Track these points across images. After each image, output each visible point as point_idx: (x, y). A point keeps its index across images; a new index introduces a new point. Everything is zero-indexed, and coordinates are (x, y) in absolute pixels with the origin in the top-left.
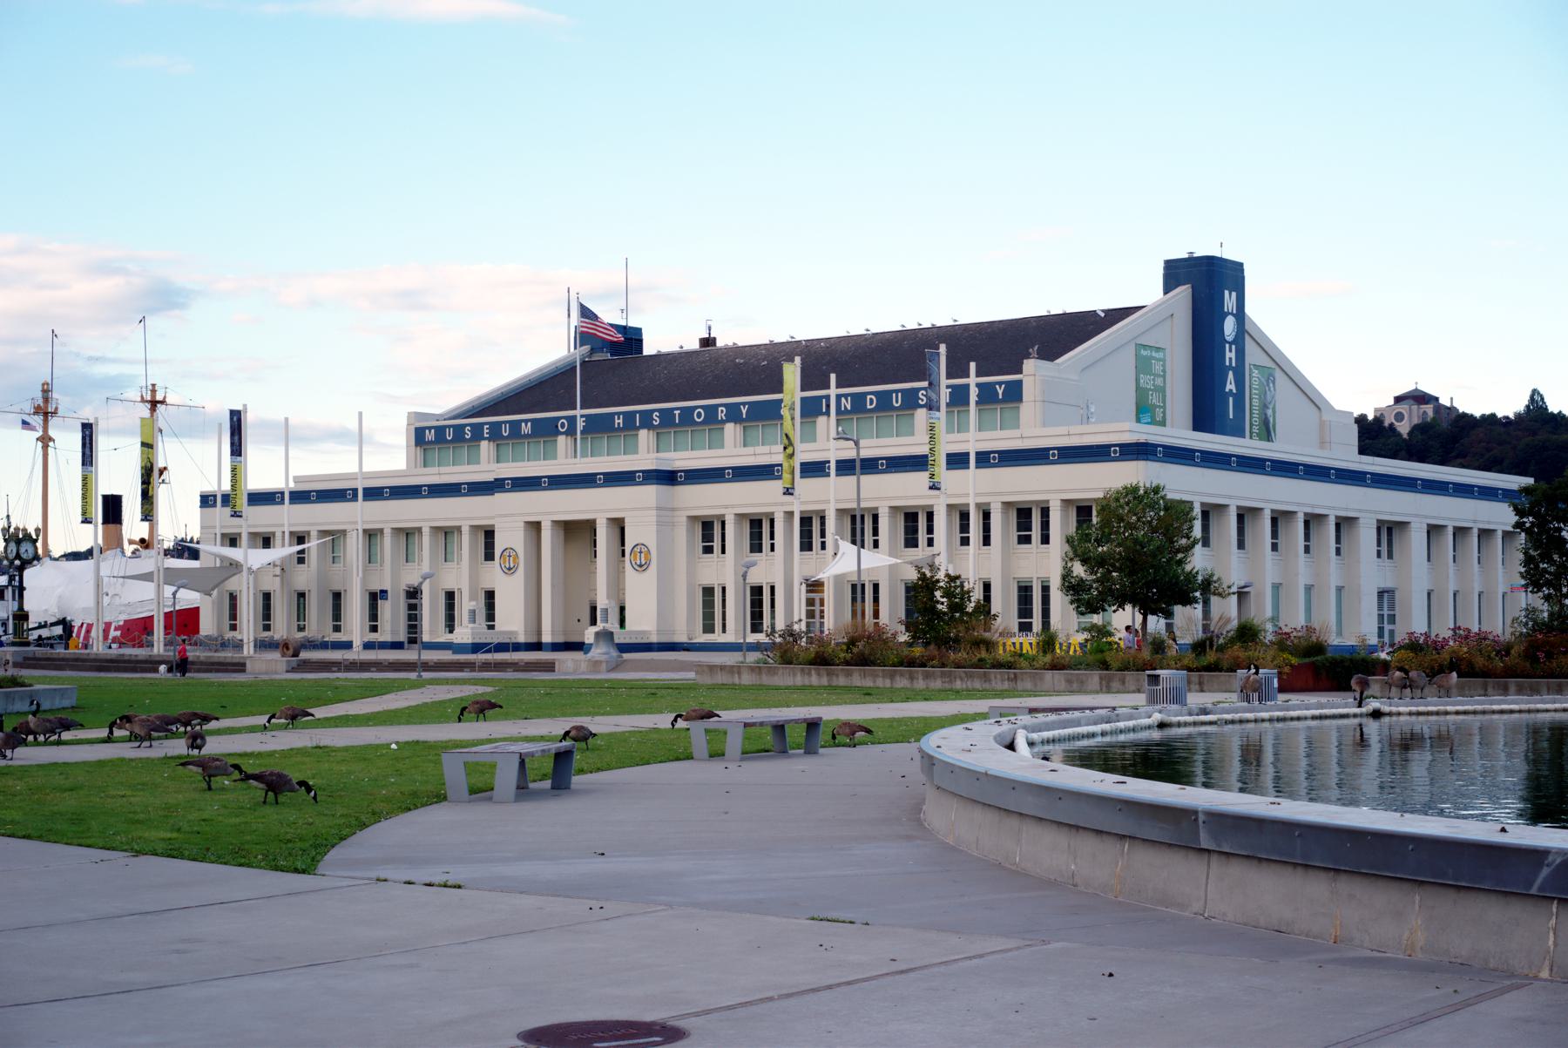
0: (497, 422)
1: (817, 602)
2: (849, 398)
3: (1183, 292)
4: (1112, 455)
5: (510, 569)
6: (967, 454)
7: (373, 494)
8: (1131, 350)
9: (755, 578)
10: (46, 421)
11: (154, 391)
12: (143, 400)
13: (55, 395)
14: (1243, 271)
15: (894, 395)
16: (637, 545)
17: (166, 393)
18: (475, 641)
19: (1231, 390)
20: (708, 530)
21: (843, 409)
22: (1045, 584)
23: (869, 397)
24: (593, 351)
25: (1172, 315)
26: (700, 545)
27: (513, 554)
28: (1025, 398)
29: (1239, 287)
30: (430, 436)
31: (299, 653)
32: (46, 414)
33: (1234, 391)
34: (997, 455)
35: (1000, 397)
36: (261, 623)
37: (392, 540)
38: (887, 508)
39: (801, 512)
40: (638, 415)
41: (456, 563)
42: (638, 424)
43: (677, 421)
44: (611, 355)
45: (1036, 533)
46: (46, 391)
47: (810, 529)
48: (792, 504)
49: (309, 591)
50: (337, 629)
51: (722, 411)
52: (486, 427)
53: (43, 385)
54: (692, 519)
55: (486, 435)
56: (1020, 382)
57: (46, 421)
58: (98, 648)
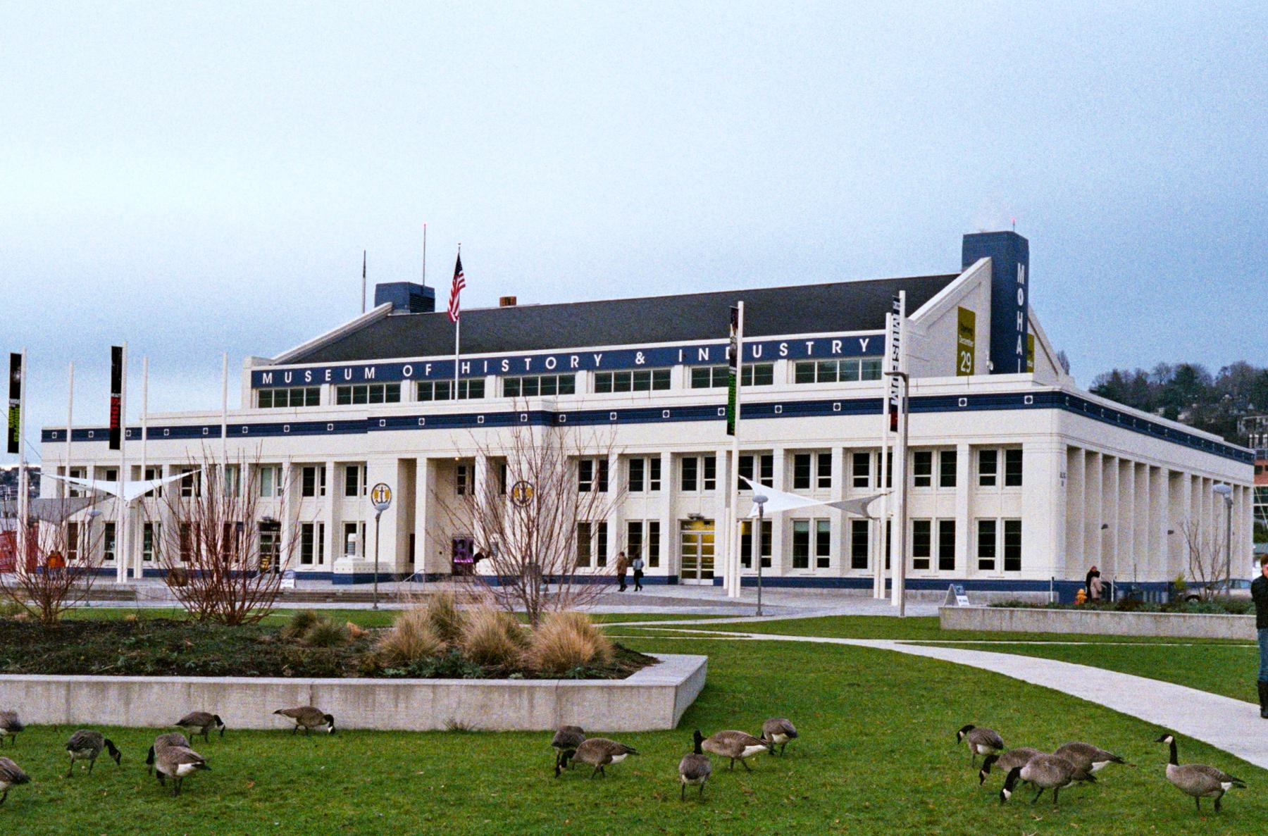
2: (707, 349)
6: (220, 427)
7: (234, 431)
8: (955, 312)
9: (307, 517)
18: (358, 572)
22: (823, 529)
24: (394, 307)
26: (851, 477)
27: (385, 488)
30: (267, 379)
34: (966, 399)
37: (428, 470)
39: (741, 452)
41: (273, 496)
43: (528, 368)
44: (412, 311)
48: (731, 443)
51: (837, 345)
52: (327, 371)
55: (327, 379)
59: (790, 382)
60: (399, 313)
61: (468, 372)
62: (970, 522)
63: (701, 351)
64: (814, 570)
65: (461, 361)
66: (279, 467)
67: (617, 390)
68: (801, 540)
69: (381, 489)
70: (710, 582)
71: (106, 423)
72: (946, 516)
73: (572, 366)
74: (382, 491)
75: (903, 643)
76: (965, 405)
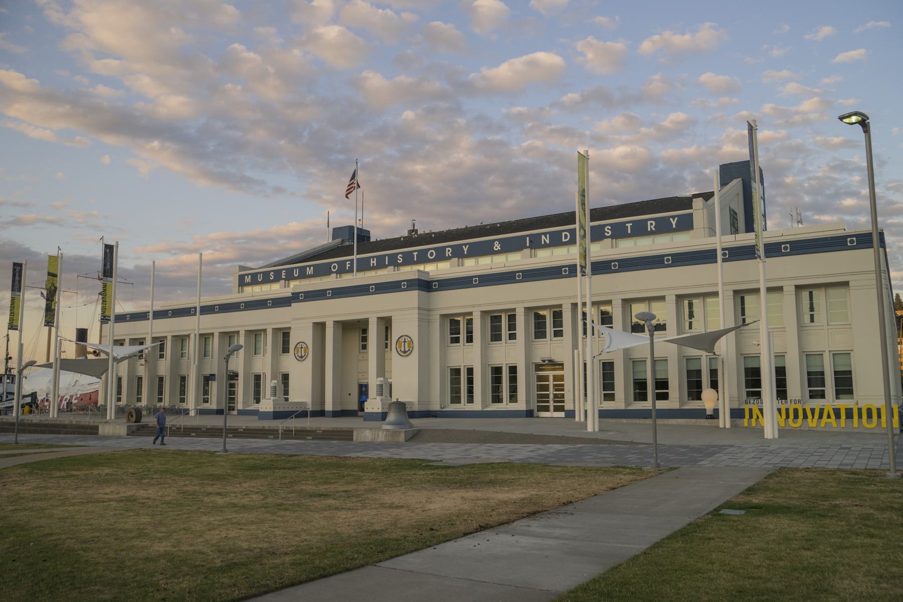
2: (548, 235)
4: (517, 278)
5: (301, 357)
15: (295, 270)
16: (299, 343)
21: (543, 243)
23: (563, 234)
27: (408, 339)
30: (248, 279)
35: (674, 227)
38: (480, 312)
39: (718, 297)
40: (387, 257)
42: (387, 263)
43: (629, 232)
45: (463, 336)
49: (165, 376)
51: (449, 251)
52: (348, 263)
54: (443, 316)
55: (283, 277)
56: (691, 215)
61: (375, 265)
63: (543, 237)
69: (301, 345)
70: (562, 414)
74: (405, 342)
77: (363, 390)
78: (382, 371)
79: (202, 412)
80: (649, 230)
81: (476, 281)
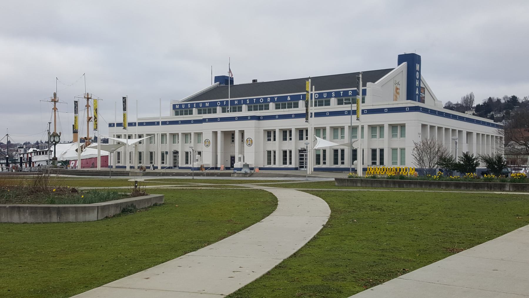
0: (240, 100)
1: (305, 156)
3: (405, 64)
7: (164, 123)
10: (55, 104)
11: (88, 95)
12: (85, 98)
13: (57, 96)
14: (420, 58)
15: (324, 94)
17: (91, 95)
19: (417, 94)
20: (270, 134)
25: (402, 71)
26: (267, 138)
28: (367, 94)
29: (419, 63)
30: (177, 107)
31: (146, 170)
32: (55, 102)
33: (418, 94)
34: (387, 109)
35: (276, 100)
36: (117, 161)
37: (169, 137)
43: (342, 95)
44: (226, 85)
45: (272, 138)
46: (55, 95)
47: (302, 133)
50: (119, 162)
52: (195, 104)
53: (54, 93)
55: (195, 107)
57: (55, 104)
58: (79, 168)
59: (336, 105)
60: (222, 85)
62: (264, 152)
64: (322, 165)
65: (315, 94)
66: (178, 134)
67: (319, 106)
68: (318, 156)
69: (207, 141)
71: (305, 112)
72: (381, 147)
73: (268, 101)
74: (249, 140)
75: (300, 190)
76: (408, 110)
77: (233, 159)
78: (242, 151)
79: (162, 168)
80: (349, 95)
81: (386, 110)
